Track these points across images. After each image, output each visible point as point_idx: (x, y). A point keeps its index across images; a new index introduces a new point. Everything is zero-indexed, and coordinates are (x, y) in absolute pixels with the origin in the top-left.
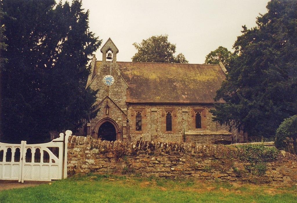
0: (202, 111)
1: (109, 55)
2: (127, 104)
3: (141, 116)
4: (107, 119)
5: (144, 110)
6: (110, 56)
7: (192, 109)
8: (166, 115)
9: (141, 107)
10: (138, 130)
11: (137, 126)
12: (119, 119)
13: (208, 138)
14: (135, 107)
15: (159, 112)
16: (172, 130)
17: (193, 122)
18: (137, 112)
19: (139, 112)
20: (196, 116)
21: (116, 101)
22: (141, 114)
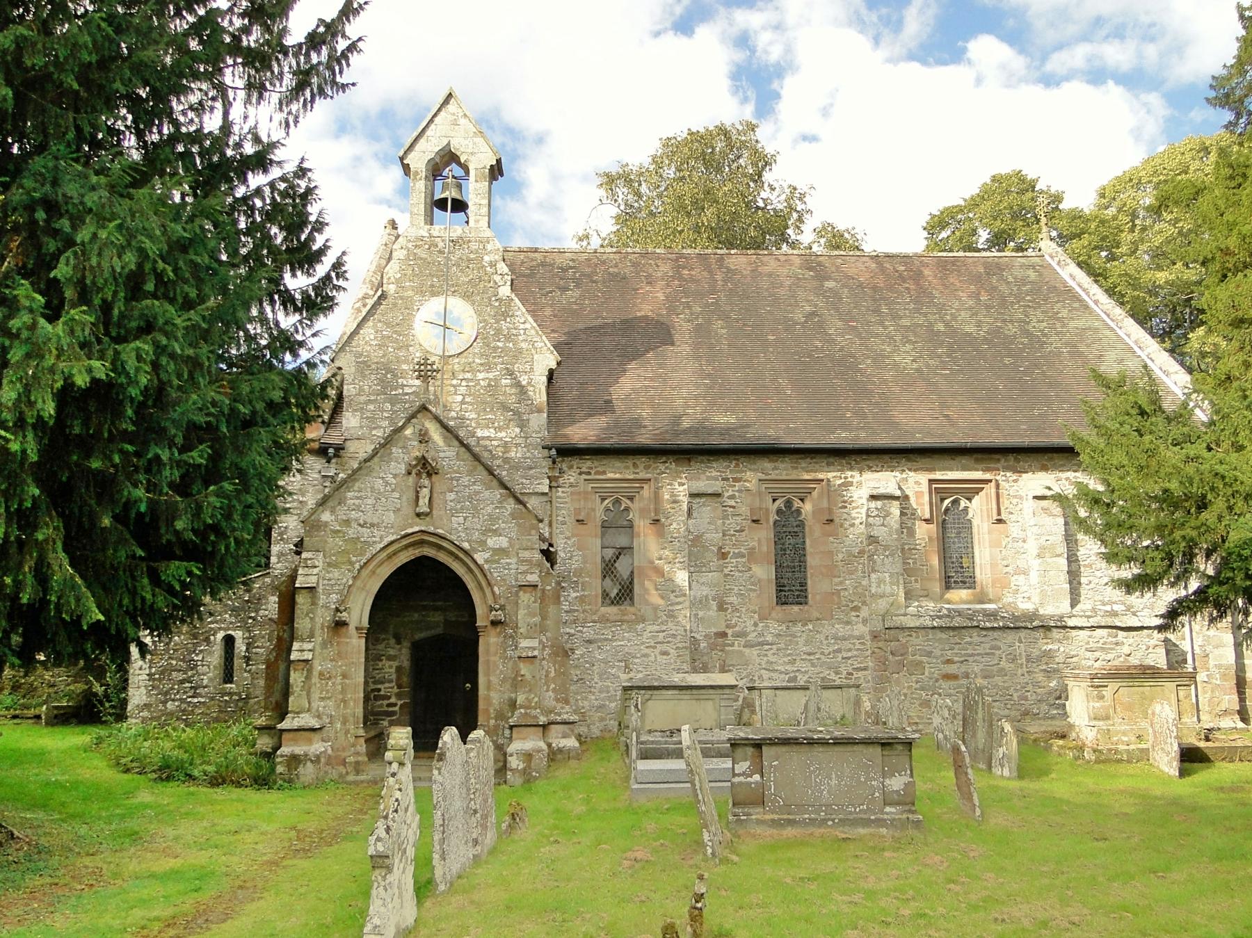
4: (422, 543)
8: (773, 517)
10: (617, 601)
11: (608, 580)
12: (492, 542)
14: (596, 473)
21: (488, 438)
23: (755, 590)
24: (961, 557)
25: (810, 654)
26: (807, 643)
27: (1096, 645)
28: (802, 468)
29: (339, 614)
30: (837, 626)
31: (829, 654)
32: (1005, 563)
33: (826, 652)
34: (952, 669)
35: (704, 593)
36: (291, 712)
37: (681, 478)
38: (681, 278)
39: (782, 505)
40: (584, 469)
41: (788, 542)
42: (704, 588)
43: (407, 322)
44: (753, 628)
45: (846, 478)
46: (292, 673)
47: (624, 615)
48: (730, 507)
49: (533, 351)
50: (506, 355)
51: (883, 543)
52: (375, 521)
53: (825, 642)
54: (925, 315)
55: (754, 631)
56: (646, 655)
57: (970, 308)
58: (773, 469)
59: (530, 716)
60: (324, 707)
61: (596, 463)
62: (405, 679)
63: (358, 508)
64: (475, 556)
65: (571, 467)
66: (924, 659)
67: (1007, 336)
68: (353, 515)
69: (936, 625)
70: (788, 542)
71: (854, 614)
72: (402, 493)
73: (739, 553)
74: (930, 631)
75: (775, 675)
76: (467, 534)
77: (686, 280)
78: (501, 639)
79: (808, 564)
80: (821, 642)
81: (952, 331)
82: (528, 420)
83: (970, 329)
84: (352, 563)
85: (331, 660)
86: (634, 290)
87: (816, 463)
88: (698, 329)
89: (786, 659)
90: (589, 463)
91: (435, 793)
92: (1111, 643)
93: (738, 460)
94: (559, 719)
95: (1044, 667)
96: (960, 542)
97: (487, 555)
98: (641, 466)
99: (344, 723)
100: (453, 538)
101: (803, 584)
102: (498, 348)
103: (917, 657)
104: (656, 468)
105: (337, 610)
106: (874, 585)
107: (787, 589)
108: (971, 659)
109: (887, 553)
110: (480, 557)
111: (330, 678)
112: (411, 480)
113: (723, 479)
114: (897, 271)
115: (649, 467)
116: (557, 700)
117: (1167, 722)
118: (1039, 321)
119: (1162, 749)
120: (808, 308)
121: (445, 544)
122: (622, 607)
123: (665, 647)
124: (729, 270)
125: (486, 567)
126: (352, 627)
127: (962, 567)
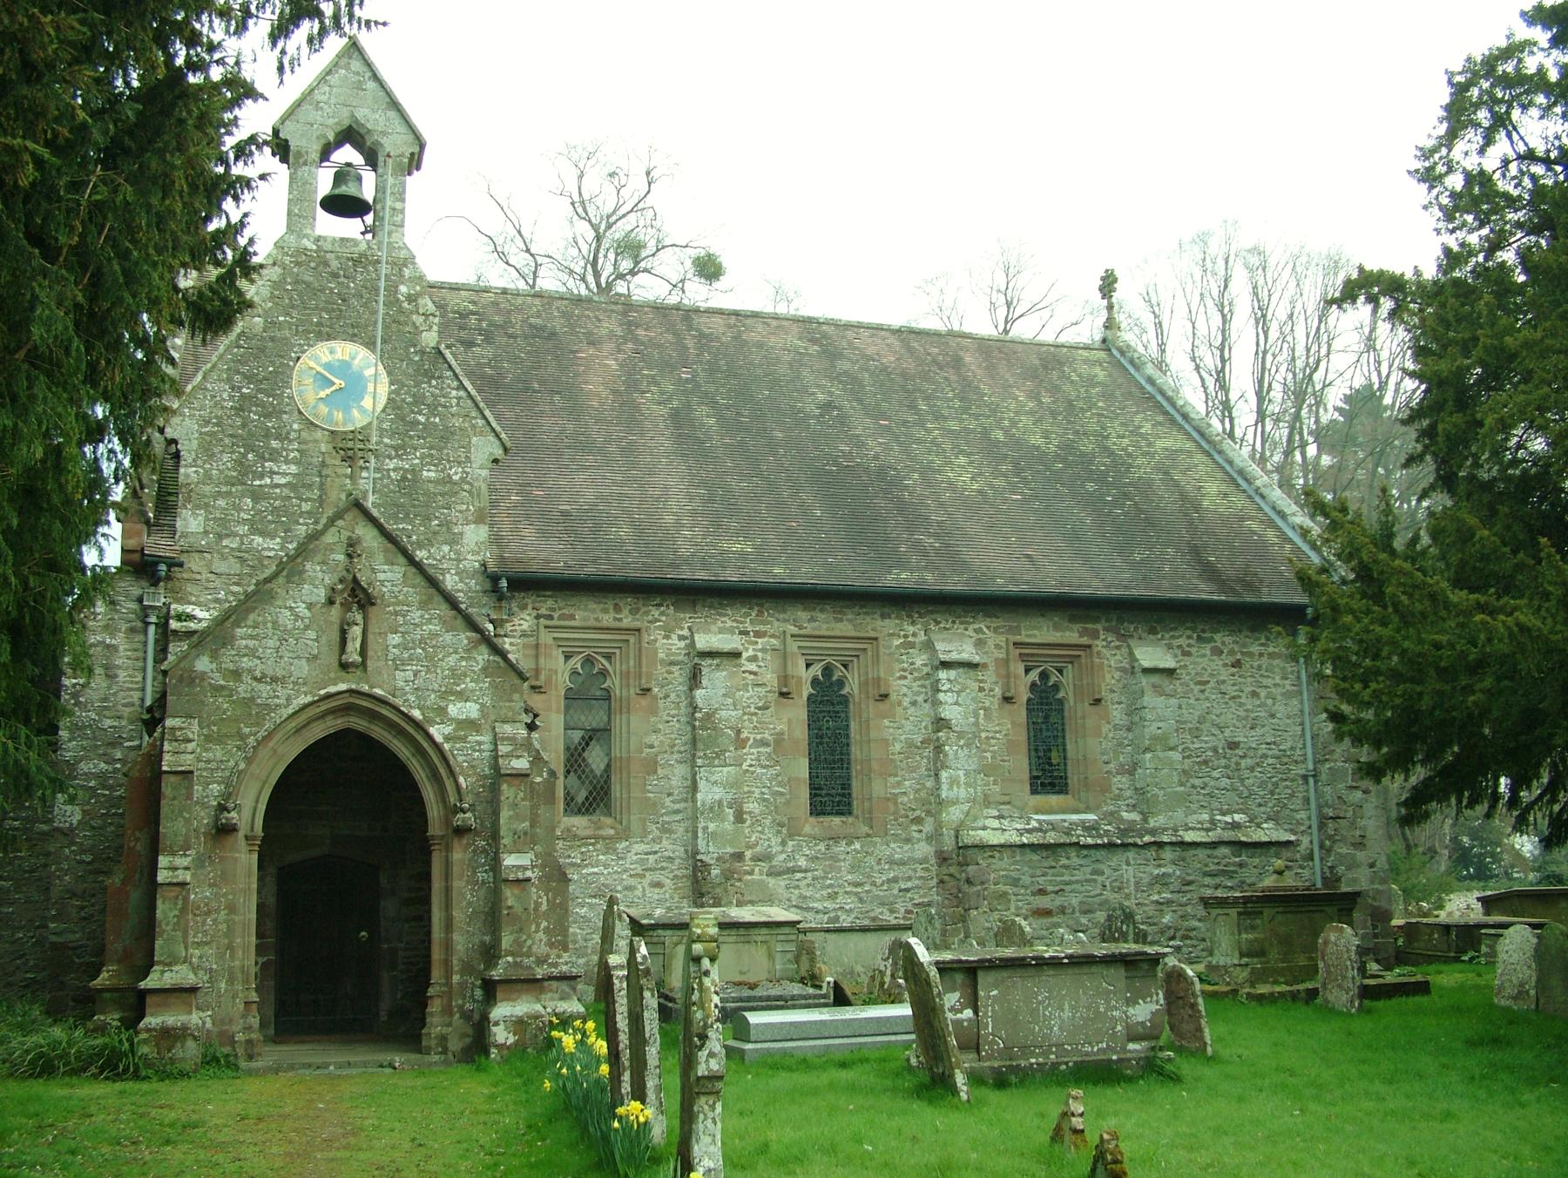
0: (1072, 660)
1: (340, 178)
2: (495, 589)
3: (607, 697)
5: (632, 639)
6: (349, 189)
7: (1001, 639)
8: (807, 690)
9: (608, 619)
10: (586, 808)
12: (454, 710)
13: (1129, 873)
14: (561, 618)
15: (753, 659)
16: (850, 813)
17: (1011, 746)
18: (576, 661)
19: (589, 661)
20: (1029, 700)
22: (604, 674)
23: (782, 794)
24: (1050, 750)
25: (857, 885)
26: (853, 868)
27: (1217, 867)
28: (850, 621)
29: (226, 814)
30: (892, 845)
31: (882, 885)
32: (1105, 758)
33: (879, 881)
35: (717, 797)
36: (159, 963)
37: (682, 629)
38: (636, 340)
39: (819, 673)
40: (543, 611)
41: (826, 726)
42: (716, 789)
43: (281, 377)
44: (780, 848)
45: (906, 636)
46: (159, 903)
47: (599, 828)
48: (751, 673)
49: (471, 433)
50: (430, 435)
52: (280, 673)
53: (876, 868)
54: (977, 416)
55: (782, 852)
56: (629, 888)
57: (1032, 413)
58: (809, 621)
59: (522, 967)
60: (201, 957)
61: (561, 604)
62: (270, 924)
63: (252, 653)
64: (432, 730)
65: (523, 607)
66: (1008, 889)
67: (1083, 455)
68: (246, 663)
69: (1025, 841)
70: (826, 726)
71: (914, 828)
72: (321, 631)
73: (761, 740)
74: (1018, 850)
75: (810, 916)
76: (418, 697)
77: (643, 344)
78: (469, 855)
79: (853, 757)
80: (872, 868)
81: (1018, 443)
82: (461, 534)
83: (1037, 440)
84: (242, 737)
85: (210, 885)
86: (572, 352)
88: (675, 415)
89: (824, 893)
90: (550, 602)
91: (647, 1023)
92: (1234, 864)
93: (761, 605)
94: (555, 971)
95: (1156, 897)
96: (1048, 730)
97: (448, 730)
98: (626, 612)
99: (231, 981)
100: (398, 702)
101: (846, 786)
102: (419, 423)
103: (1001, 887)
104: (647, 613)
105: (222, 808)
106: (944, 787)
107: (824, 792)
108: (1067, 888)
109: (962, 743)
110: (437, 732)
111: (208, 913)
112: (335, 611)
113: (741, 633)
114: (929, 354)
115: (638, 610)
116: (551, 945)
117: (1348, 951)
118: (1119, 437)
119: (1339, 986)
120: (821, 396)
121: (385, 712)
122: (594, 818)
123: (657, 877)
124: (702, 335)
125: (447, 746)
126: (241, 834)
127: (1051, 764)
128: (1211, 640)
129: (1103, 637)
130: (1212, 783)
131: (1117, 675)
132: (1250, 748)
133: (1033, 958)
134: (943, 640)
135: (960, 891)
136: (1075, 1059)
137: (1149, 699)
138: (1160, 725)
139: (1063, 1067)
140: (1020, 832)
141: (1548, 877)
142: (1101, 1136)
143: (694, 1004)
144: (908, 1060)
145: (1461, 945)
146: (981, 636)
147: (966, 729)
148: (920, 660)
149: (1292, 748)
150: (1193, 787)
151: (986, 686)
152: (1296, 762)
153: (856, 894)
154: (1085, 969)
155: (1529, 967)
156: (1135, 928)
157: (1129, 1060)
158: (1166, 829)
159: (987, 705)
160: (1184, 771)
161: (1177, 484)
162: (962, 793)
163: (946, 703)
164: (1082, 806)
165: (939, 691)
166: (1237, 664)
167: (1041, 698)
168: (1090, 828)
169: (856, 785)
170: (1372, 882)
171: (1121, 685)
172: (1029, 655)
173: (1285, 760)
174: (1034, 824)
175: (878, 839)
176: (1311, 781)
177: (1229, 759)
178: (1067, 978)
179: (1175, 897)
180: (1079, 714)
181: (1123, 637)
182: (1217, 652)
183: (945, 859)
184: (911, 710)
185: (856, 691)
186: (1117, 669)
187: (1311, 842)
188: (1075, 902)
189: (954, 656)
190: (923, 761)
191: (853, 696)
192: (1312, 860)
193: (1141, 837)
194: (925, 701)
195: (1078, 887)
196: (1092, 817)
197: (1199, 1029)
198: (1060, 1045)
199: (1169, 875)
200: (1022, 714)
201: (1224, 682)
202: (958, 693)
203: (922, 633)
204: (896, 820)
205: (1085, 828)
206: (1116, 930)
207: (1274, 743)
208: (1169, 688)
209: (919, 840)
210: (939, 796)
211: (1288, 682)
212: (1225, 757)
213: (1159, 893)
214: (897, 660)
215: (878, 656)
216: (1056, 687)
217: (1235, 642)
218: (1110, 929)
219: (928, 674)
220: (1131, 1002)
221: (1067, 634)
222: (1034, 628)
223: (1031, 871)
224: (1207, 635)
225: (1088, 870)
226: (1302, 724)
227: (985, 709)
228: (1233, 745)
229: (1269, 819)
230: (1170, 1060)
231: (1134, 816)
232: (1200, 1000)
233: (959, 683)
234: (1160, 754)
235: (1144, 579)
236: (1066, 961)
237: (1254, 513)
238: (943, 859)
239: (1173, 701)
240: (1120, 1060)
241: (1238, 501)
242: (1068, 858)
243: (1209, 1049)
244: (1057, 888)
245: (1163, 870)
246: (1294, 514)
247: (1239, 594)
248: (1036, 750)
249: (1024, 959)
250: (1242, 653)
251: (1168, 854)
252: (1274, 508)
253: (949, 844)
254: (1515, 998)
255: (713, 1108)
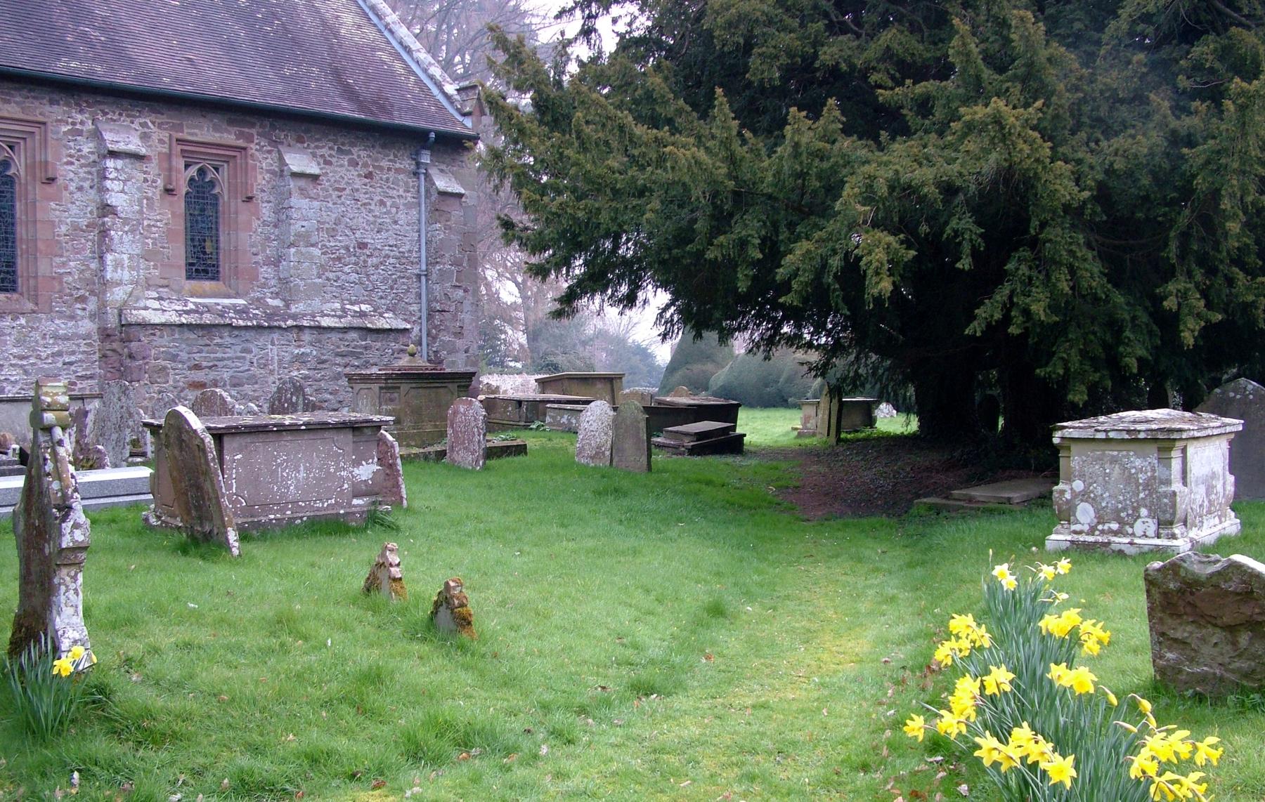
0: (227, 160)
7: (165, 135)
13: (273, 352)
16: (14, 290)
17: (170, 233)
20: (187, 193)
24: (204, 241)
25: (22, 358)
26: (18, 343)
28: (16, 103)
30: (57, 321)
31: (46, 358)
32: (254, 250)
33: (44, 355)
34: (199, 376)
45: (74, 124)
51: (122, 215)
53: (42, 342)
69: (185, 321)
71: (78, 306)
74: (177, 329)
79: (18, 236)
80: (37, 342)
87: (34, 98)
92: (361, 347)
96: (203, 222)
101: (11, 264)
106: (109, 269)
109: (127, 228)
117: (476, 420)
119: (465, 448)
127: (205, 253)
128: (349, 152)
129: (256, 141)
130: (343, 277)
131: (267, 176)
132: (376, 249)
133: (275, 425)
134: (111, 131)
135: (122, 365)
136: (308, 514)
137: (296, 201)
138: (304, 223)
139: (298, 521)
140: (180, 314)
141: (548, 365)
142: (447, 583)
143: (49, 474)
144: (146, 520)
145: (529, 416)
146: (146, 130)
147: (130, 216)
148: (87, 147)
149: (410, 251)
150: (328, 279)
151: (150, 177)
152: (412, 263)
153: (22, 366)
154: (319, 435)
155: (606, 434)
156: (305, 399)
157: (354, 513)
158: (305, 315)
159: (150, 195)
160: (321, 265)
161: (317, 11)
162: (126, 275)
163: (113, 190)
164: (232, 292)
165: (106, 178)
166: (369, 176)
167: (198, 192)
168: (242, 312)
169: (21, 264)
170: (466, 366)
171: (270, 186)
172: (190, 151)
173: (403, 261)
174: (191, 306)
175: (43, 316)
176: (423, 279)
177: (358, 257)
178: (303, 441)
179: (311, 373)
180: (232, 210)
181: (275, 143)
182: (354, 164)
183: (108, 336)
184: (78, 195)
185: (22, 173)
186: (268, 171)
187: (421, 330)
188: (226, 376)
189: (121, 147)
190: (88, 244)
191: (19, 178)
192: (420, 344)
193: (285, 321)
194: (91, 187)
195: (229, 363)
196: (241, 301)
197: (398, 486)
198: (295, 502)
199: (307, 355)
200: (182, 205)
201: (357, 190)
202: (125, 182)
203: (90, 122)
204: (61, 298)
205: (236, 312)
206: (286, 401)
207: (396, 246)
208: (313, 192)
209: (83, 318)
210: (103, 277)
211: (409, 194)
212: (355, 255)
213: (298, 369)
214: (65, 146)
215: (46, 140)
216: (212, 184)
217: (369, 156)
218: (280, 401)
219: (94, 162)
220: (357, 463)
221: (225, 135)
222: (196, 127)
223: (188, 348)
224: (346, 148)
225: (239, 348)
226: (419, 231)
227: (148, 199)
228: (362, 246)
229: (388, 310)
230: (388, 513)
231: (277, 302)
232: (399, 461)
233: (126, 173)
234: (303, 250)
235: (295, 91)
236: (303, 427)
237: (383, 46)
238: (106, 335)
239: (316, 204)
240: (346, 514)
241: (371, 34)
242: (221, 338)
243: (405, 502)
244: (211, 364)
245: (302, 350)
246: (418, 51)
247: (372, 113)
248: (192, 240)
249: (266, 426)
250: (374, 166)
251: (307, 337)
252: (401, 43)
253: (112, 321)
254: (592, 458)
255: (75, 579)
